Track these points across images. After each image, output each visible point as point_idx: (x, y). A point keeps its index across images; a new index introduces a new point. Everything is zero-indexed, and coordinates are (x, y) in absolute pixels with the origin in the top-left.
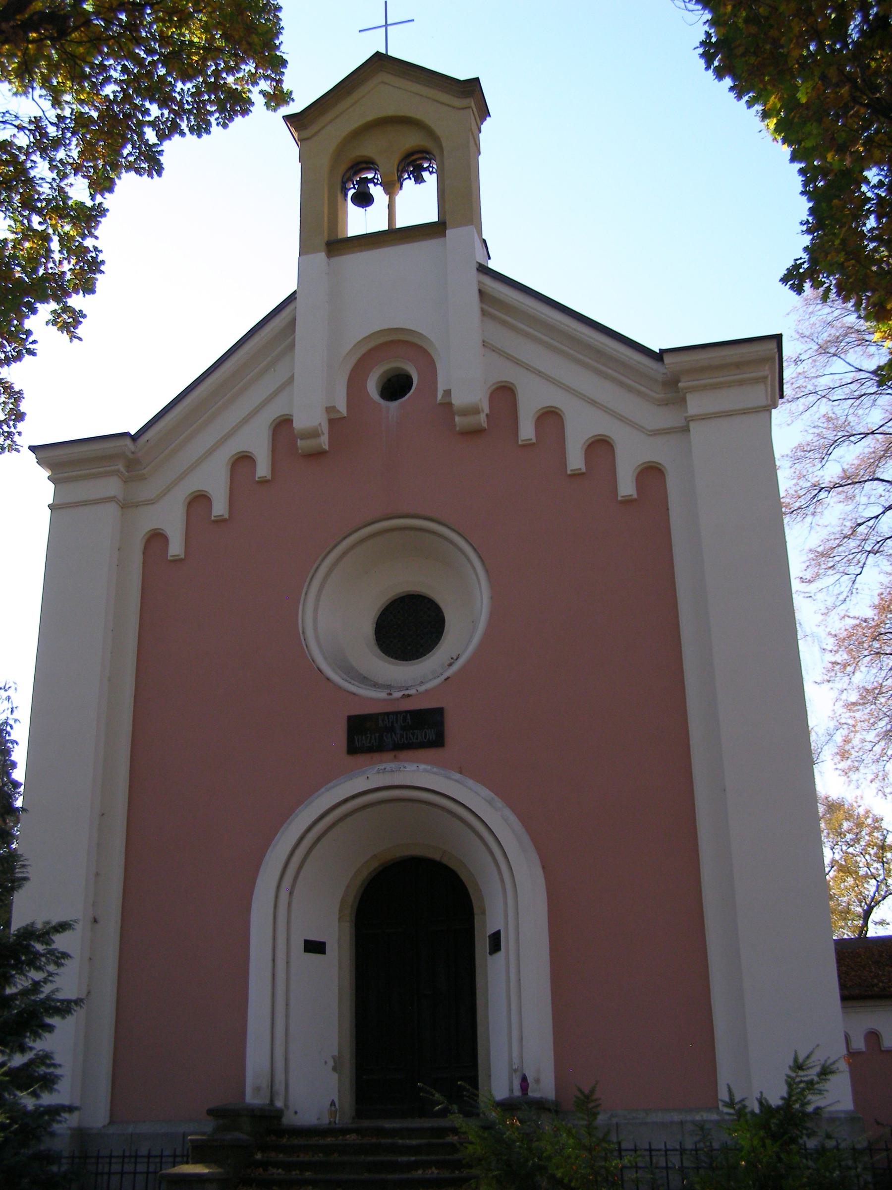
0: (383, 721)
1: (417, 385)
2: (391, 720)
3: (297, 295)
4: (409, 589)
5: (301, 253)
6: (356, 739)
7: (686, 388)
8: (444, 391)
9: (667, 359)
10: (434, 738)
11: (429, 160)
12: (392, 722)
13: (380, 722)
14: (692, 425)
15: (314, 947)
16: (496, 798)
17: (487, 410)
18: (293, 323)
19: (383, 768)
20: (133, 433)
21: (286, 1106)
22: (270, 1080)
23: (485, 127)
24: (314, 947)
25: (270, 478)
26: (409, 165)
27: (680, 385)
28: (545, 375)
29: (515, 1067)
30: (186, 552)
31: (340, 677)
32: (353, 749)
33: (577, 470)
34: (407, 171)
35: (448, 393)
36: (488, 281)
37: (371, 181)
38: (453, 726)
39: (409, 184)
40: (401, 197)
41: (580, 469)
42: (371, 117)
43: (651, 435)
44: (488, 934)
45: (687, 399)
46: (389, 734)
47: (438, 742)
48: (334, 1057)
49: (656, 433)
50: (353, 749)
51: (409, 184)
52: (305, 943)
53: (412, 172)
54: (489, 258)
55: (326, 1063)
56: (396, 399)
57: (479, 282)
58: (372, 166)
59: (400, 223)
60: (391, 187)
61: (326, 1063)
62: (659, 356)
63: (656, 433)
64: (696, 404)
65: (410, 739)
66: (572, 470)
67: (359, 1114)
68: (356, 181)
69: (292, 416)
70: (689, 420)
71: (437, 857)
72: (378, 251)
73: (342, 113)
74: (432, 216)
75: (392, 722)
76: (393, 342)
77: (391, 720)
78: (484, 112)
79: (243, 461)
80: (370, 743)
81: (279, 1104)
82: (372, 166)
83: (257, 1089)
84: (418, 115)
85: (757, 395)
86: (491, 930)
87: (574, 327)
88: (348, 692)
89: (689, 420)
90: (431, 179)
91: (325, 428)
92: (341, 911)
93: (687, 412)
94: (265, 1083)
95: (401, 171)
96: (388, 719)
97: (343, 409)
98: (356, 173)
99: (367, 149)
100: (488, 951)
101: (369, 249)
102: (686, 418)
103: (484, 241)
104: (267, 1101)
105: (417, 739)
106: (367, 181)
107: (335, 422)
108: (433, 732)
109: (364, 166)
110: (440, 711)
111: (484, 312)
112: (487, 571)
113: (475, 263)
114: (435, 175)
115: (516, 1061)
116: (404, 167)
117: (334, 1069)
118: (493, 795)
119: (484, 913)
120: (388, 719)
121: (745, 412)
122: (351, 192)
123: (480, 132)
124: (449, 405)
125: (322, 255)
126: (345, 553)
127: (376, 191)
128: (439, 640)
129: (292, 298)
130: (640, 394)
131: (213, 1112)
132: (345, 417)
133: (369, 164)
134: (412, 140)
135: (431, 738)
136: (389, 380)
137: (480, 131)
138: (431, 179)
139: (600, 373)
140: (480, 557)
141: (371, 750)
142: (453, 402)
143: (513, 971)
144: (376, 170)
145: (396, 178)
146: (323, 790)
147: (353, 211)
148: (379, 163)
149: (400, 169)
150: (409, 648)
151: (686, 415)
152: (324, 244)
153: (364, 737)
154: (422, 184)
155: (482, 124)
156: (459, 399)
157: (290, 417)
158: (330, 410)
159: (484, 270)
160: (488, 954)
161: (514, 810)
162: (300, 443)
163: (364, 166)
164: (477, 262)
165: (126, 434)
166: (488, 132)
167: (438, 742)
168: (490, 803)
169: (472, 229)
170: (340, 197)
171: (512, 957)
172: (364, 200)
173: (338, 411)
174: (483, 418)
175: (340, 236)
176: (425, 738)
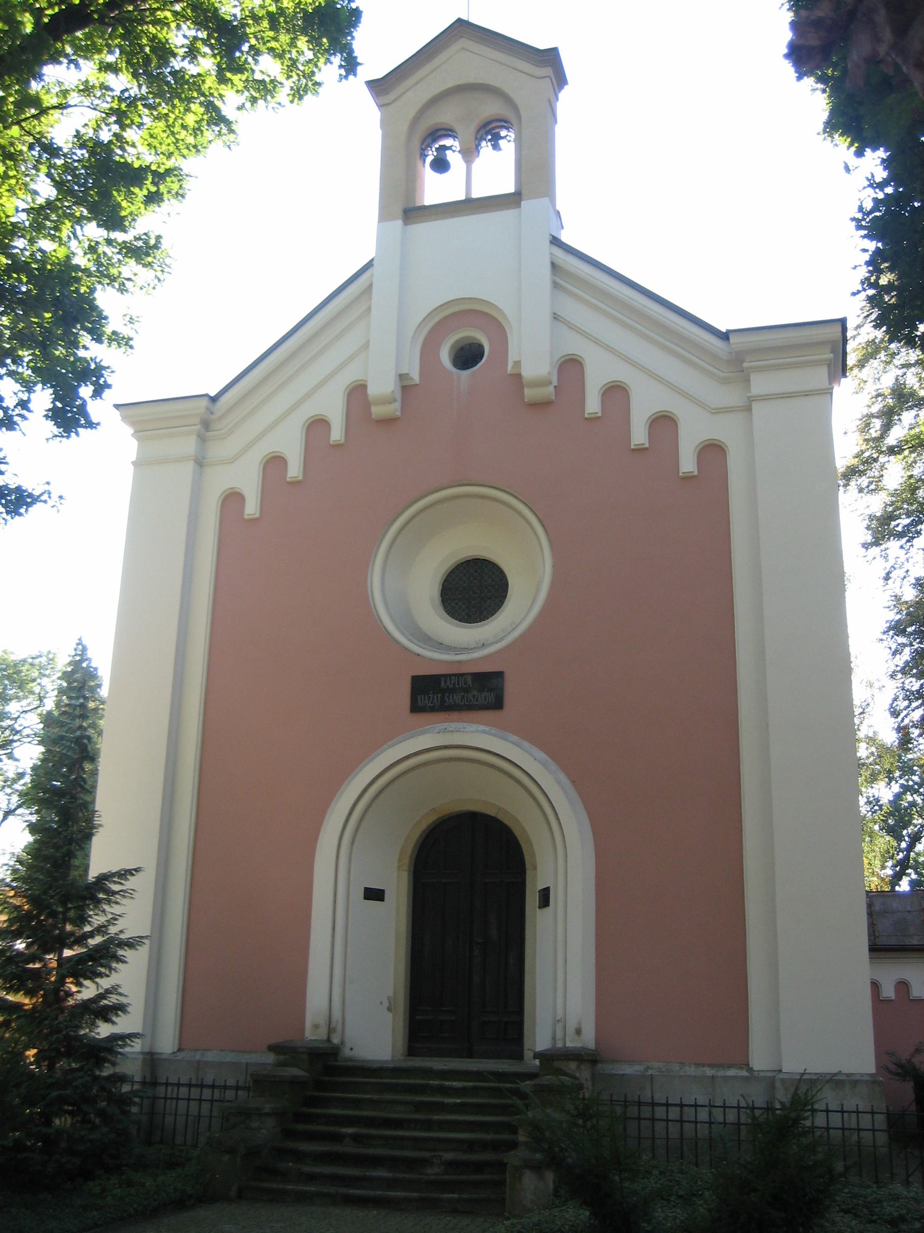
0: (445, 682)
1: (488, 355)
2: (453, 682)
3: (375, 262)
4: (477, 553)
5: (380, 221)
6: (419, 698)
7: (751, 368)
8: (515, 362)
9: (733, 339)
10: (493, 701)
11: (507, 128)
12: (454, 684)
13: (443, 683)
14: (755, 406)
15: (374, 895)
16: (550, 761)
17: (555, 383)
18: (369, 288)
19: (444, 727)
20: (212, 394)
21: (343, 1043)
22: (328, 1020)
23: (562, 95)
24: (374, 895)
25: (400, 415)
26: (487, 133)
27: (745, 365)
28: (613, 349)
29: (558, 1018)
30: (261, 511)
31: (406, 637)
32: (416, 708)
33: (640, 445)
34: (485, 140)
35: (517, 364)
36: (559, 253)
37: (450, 148)
38: (511, 689)
39: (486, 148)
40: (477, 164)
41: (643, 444)
42: (450, 84)
43: (714, 413)
44: (538, 890)
45: (751, 378)
46: (451, 695)
47: (498, 704)
48: (389, 998)
49: (718, 411)
50: (416, 708)
51: (486, 148)
52: (365, 891)
53: (490, 140)
54: (563, 228)
55: (381, 1003)
56: (468, 368)
57: (551, 254)
58: (451, 133)
59: (475, 195)
60: (469, 154)
61: (381, 1003)
62: (725, 336)
63: (718, 411)
64: (760, 384)
65: (471, 701)
66: (635, 445)
67: (411, 1052)
68: (436, 148)
69: (366, 381)
70: (751, 400)
71: (492, 812)
72: (456, 219)
73: (422, 79)
74: (509, 187)
75: (454, 684)
76: (613, 387)
77: (453, 682)
78: (560, 80)
79: (319, 425)
80: (432, 703)
81: (336, 1040)
82: (451, 133)
83: (316, 1026)
84: (497, 83)
85: (820, 376)
86: (541, 887)
87: (644, 303)
88: (412, 652)
89: (751, 400)
90: (508, 146)
91: (398, 396)
92: (400, 860)
93: (750, 392)
94: (322, 1021)
95: (479, 139)
96: (450, 680)
97: (416, 377)
98: (435, 140)
99: (445, 115)
100: (538, 905)
101: (443, 219)
102: (749, 397)
103: (558, 212)
104: (325, 1038)
105: (477, 701)
106: (444, 148)
107: (406, 388)
108: (492, 695)
109: (444, 132)
110: (499, 675)
111: (555, 285)
112: (550, 540)
113: (549, 235)
114: (512, 145)
115: (560, 1012)
116: (482, 136)
117: (389, 1009)
118: (548, 758)
119: (535, 868)
120: (450, 680)
121: (807, 394)
122: (429, 159)
123: (556, 122)
124: (519, 376)
125: (400, 222)
126: (388, 552)
127: (454, 158)
128: (503, 603)
129: (369, 265)
130: (702, 370)
131: (274, 1048)
132: (417, 385)
133: (449, 132)
134: (491, 108)
135: (490, 700)
136: (462, 349)
137: (557, 99)
138: (508, 146)
139: (663, 347)
140: (543, 526)
141: (433, 709)
142: (523, 374)
143: (560, 947)
144: (454, 137)
145: (474, 146)
146: (385, 746)
147: (429, 175)
148: (458, 132)
149: (478, 137)
150: (474, 610)
151: (748, 395)
152: (402, 212)
153: (426, 697)
154: (499, 152)
155: (560, 92)
156: (529, 372)
157: (364, 383)
158: (402, 377)
159: (555, 241)
160: (537, 908)
161: (568, 775)
162: (374, 409)
163: (444, 132)
164: (551, 235)
165: (207, 395)
166: (566, 100)
167: (498, 704)
168: (544, 765)
169: (545, 201)
170: (419, 163)
171: (560, 914)
172: (441, 165)
173: (412, 379)
174: (551, 389)
175: (418, 204)
176: (485, 701)
